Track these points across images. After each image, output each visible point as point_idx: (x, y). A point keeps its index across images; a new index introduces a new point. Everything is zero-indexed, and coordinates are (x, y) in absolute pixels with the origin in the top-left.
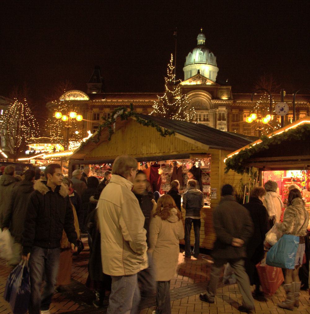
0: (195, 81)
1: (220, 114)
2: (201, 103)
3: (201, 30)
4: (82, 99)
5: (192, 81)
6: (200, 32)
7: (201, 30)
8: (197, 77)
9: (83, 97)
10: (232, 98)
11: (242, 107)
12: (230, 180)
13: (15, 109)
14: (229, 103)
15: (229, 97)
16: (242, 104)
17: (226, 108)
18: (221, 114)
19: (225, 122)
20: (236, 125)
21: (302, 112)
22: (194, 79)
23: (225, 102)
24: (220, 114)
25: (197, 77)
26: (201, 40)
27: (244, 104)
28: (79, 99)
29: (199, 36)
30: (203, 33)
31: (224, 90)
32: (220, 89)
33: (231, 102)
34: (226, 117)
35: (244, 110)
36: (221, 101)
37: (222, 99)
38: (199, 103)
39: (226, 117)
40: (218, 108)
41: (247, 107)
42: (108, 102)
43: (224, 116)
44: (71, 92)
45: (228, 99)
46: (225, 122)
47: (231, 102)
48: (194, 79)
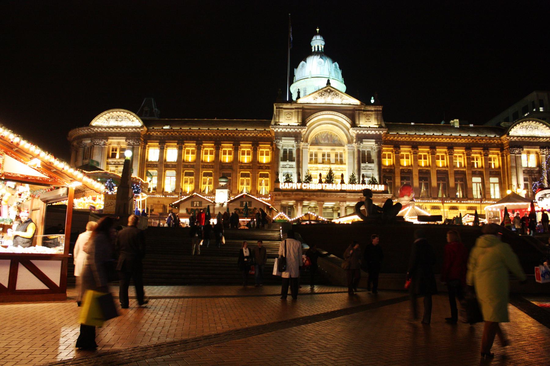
0: (323, 97)
1: (285, 151)
2: (331, 136)
3: (318, 30)
4: (130, 124)
5: (318, 97)
6: (316, 34)
7: (318, 30)
8: (326, 91)
9: (133, 121)
10: (383, 125)
11: (238, 138)
12: (181, 316)
13: (172, 154)
14: (380, 133)
15: (379, 123)
16: (398, 137)
17: (376, 142)
18: (286, 151)
19: (294, 164)
20: (389, 172)
21: (113, 139)
22: (321, 93)
23: (292, 130)
24: (285, 151)
25: (326, 91)
26: (318, 42)
27: (402, 137)
28: (125, 123)
29: (314, 38)
30: (320, 34)
31: (370, 113)
32: (364, 111)
33: (382, 132)
34: (295, 155)
35: (401, 146)
36: (360, 130)
37: (360, 127)
38: (328, 134)
39: (295, 155)
40: (107, 139)
41: (267, 138)
42: (174, 131)
43: (370, 155)
44: (111, 113)
45: (298, 125)
46: (294, 164)
47: (382, 132)
48: (321, 93)
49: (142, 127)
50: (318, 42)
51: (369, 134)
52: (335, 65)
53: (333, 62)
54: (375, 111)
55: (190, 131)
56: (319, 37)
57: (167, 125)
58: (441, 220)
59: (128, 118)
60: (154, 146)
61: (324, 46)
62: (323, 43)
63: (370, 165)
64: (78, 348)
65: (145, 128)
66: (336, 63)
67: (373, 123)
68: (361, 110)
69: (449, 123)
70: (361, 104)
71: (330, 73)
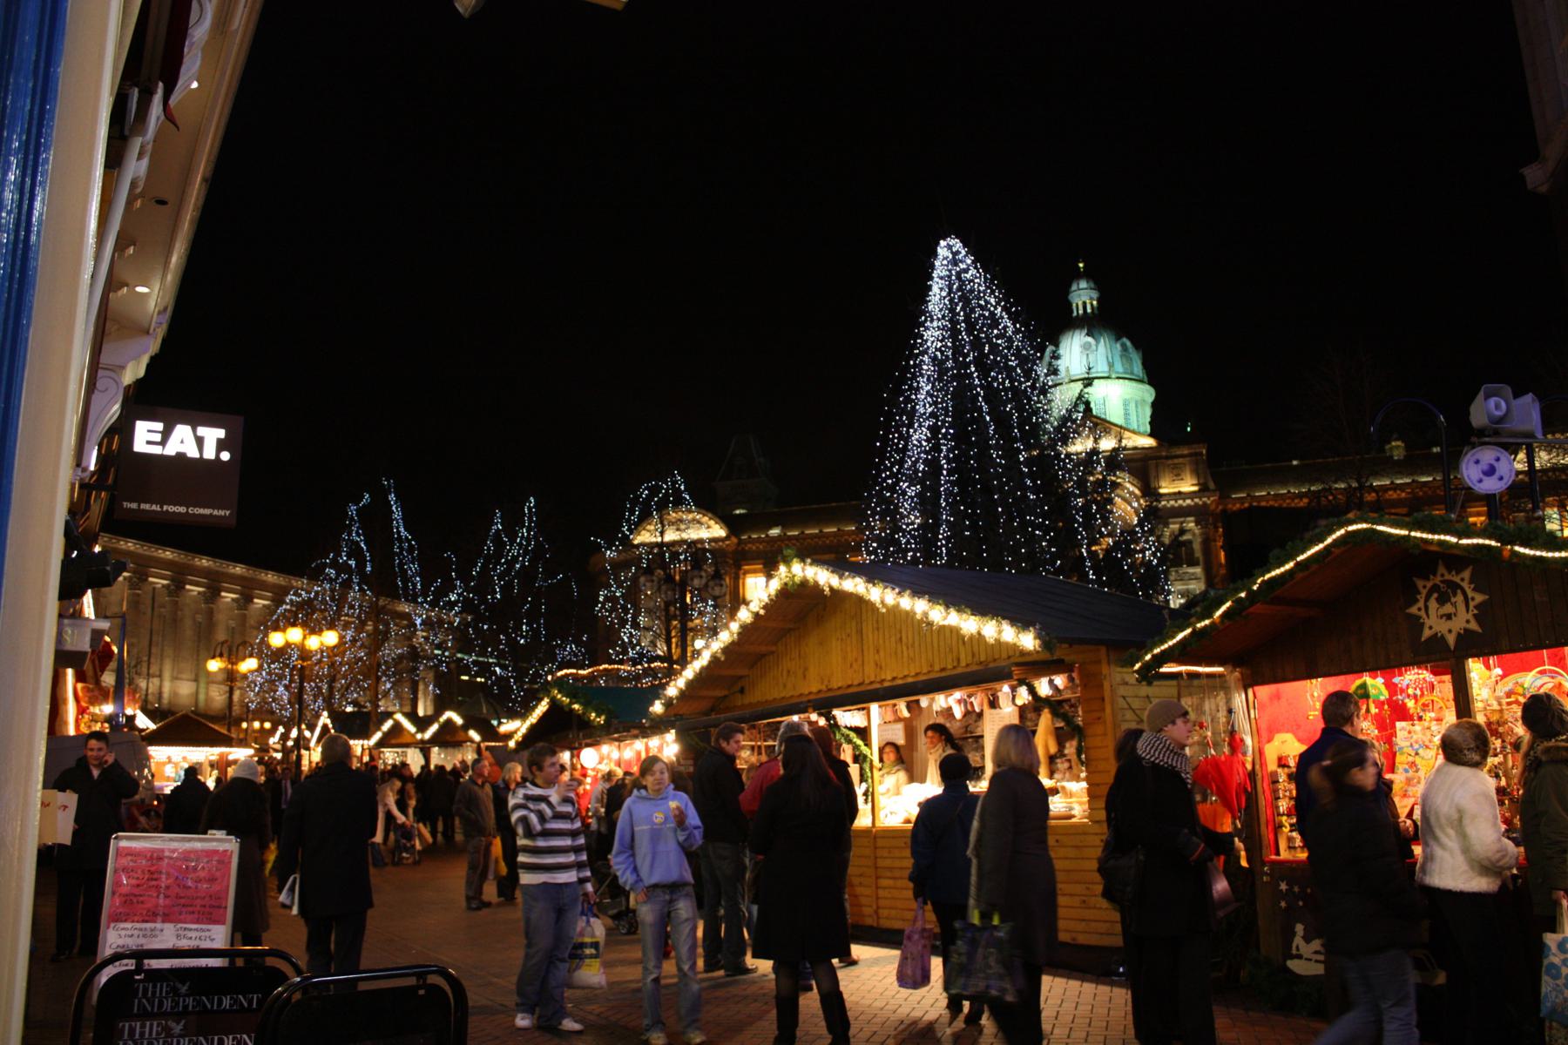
6: (1078, 276)
26: (1083, 297)
30: (1086, 274)
32: (1167, 458)
49: (727, 538)
50: (1083, 297)
51: (1181, 507)
52: (1123, 345)
53: (1117, 339)
54: (1190, 455)
55: (821, 535)
56: (1083, 284)
57: (776, 525)
58: (449, 721)
59: (699, 522)
60: (755, 572)
61: (1099, 301)
62: (1095, 294)
63: (1191, 570)
64: (762, 612)
65: (734, 540)
66: (1125, 340)
67: (1188, 486)
68: (1161, 458)
69: (1384, 451)
70: (1160, 444)
71: (1111, 365)
